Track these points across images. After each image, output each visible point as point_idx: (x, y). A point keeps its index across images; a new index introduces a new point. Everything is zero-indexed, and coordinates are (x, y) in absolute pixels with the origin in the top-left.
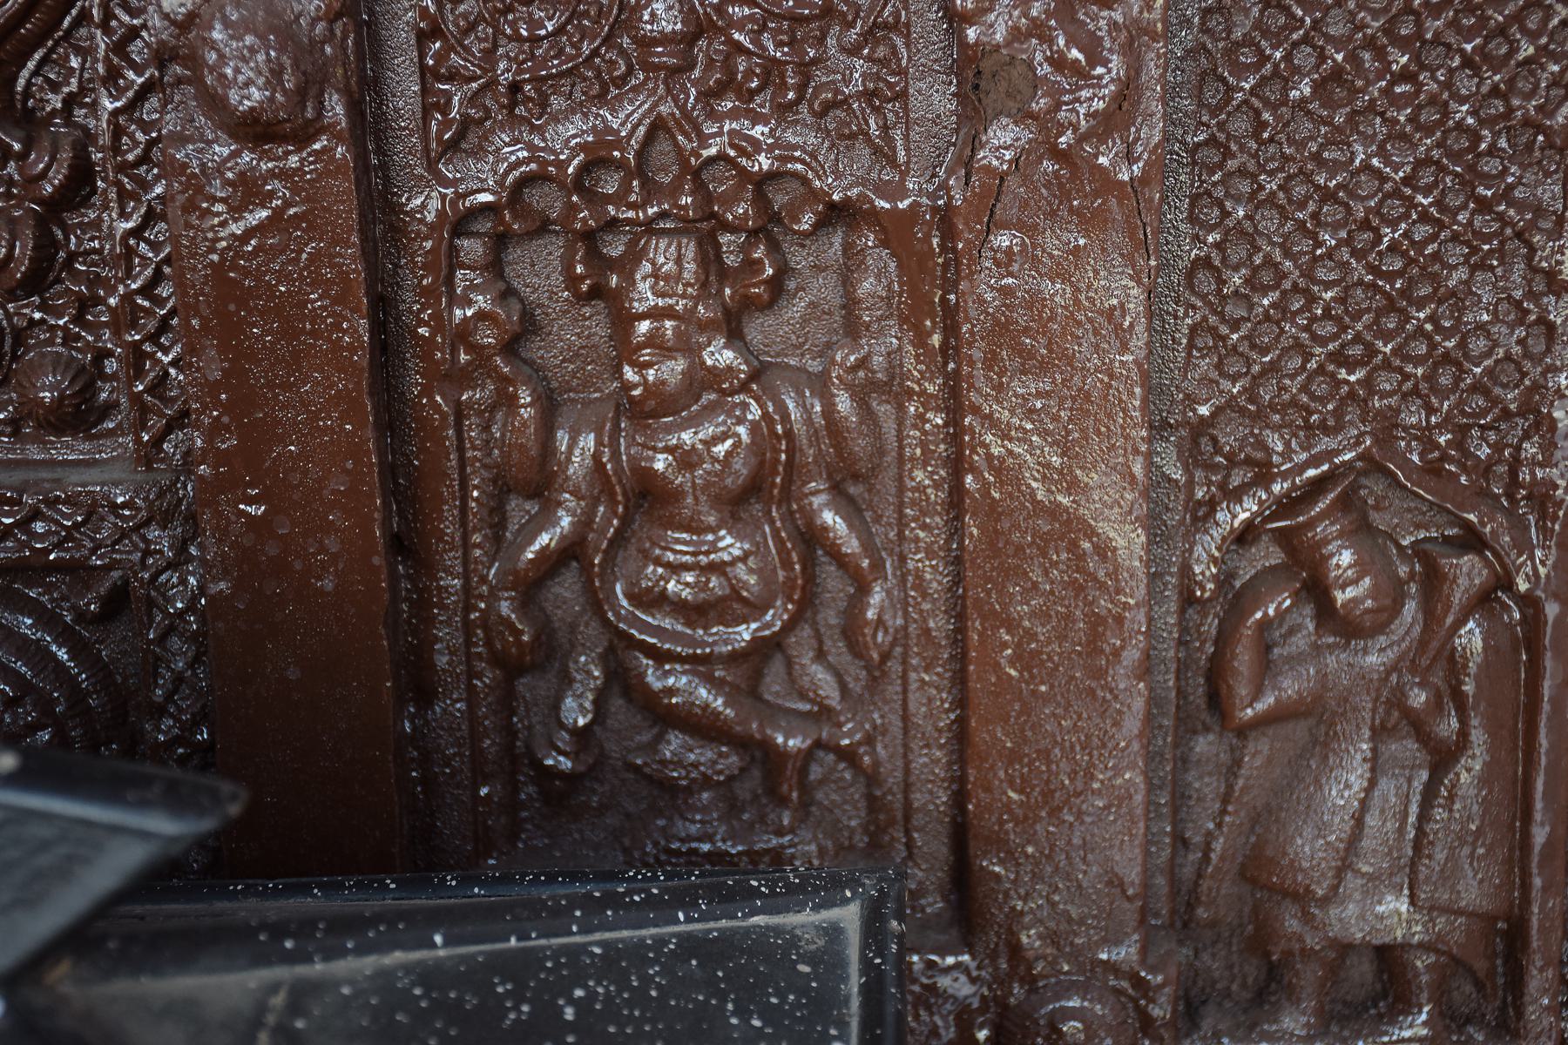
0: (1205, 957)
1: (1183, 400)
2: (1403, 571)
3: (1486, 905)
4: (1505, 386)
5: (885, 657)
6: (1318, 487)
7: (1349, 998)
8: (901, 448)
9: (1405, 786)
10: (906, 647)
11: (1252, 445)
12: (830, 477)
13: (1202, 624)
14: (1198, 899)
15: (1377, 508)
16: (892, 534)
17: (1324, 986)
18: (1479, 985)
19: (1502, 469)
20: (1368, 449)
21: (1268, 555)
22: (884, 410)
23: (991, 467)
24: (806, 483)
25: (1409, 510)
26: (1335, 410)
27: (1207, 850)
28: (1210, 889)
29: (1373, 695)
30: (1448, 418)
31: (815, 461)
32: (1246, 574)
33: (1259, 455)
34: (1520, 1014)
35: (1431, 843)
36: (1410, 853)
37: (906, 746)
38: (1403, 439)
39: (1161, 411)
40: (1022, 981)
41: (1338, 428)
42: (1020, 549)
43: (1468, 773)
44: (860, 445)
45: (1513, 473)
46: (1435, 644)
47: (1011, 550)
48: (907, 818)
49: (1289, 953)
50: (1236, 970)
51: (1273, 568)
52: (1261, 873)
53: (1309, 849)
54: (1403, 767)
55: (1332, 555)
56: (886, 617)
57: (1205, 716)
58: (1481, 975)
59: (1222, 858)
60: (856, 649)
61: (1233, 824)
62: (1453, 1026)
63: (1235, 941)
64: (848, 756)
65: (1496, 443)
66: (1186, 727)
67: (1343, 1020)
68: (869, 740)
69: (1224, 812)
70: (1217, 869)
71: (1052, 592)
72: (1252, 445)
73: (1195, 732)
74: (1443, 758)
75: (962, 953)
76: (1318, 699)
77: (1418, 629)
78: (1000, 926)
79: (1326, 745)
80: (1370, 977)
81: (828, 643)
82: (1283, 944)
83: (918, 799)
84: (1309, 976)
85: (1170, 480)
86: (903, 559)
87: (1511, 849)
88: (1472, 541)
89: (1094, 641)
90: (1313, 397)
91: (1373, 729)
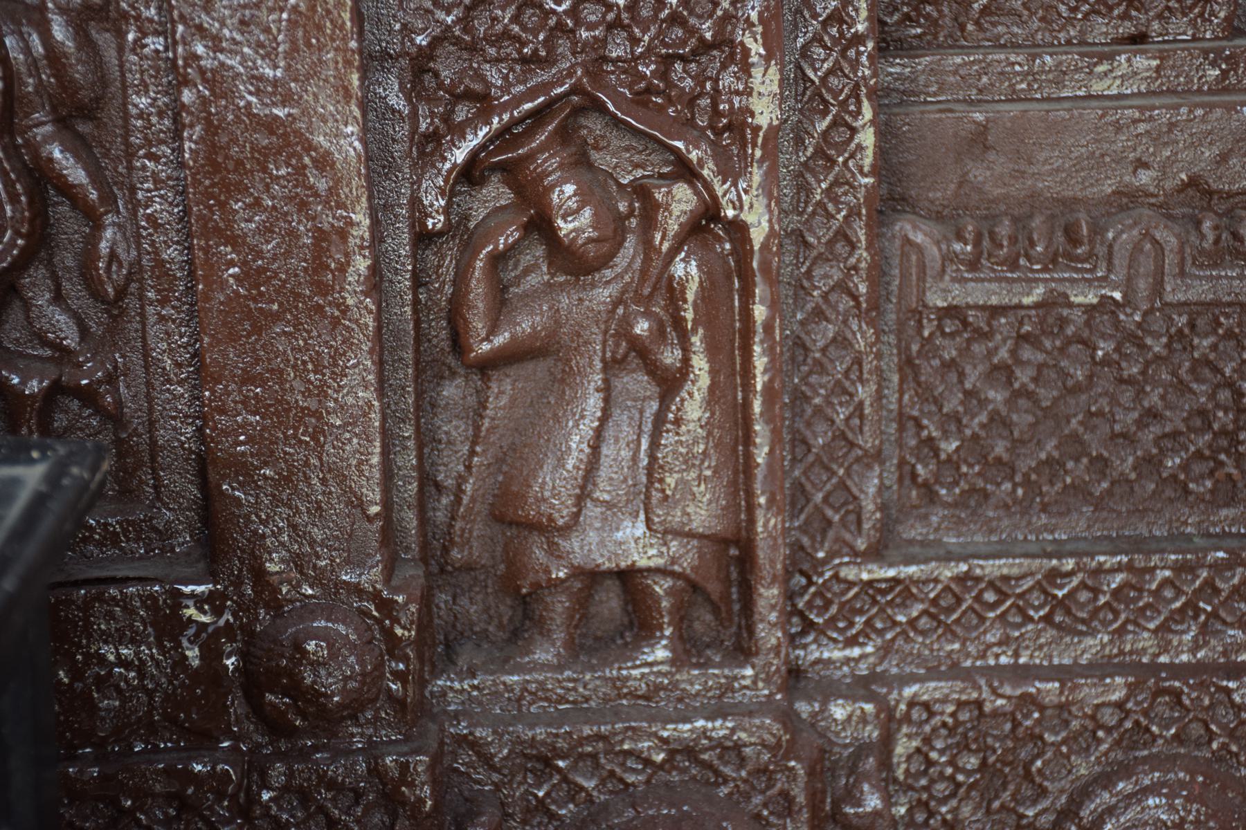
0: (464, 601)
1: (401, 31)
2: (622, 207)
3: (717, 527)
4: (700, 17)
5: (122, 293)
6: (538, 116)
7: (599, 633)
8: (123, 75)
9: (637, 416)
10: (141, 280)
11: (471, 77)
12: (54, 109)
13: (440, 266)
14: (451, 541)
15: (597, 148)
16: (120, 169)
17: (572, 617)
18: (716, 610)
19: (705, 102)
20: (580, 79)
21: (496, 193)
22: (105, 40)
23: (205, 81)
24: (27, 115)
25: (627, 149)
26: (546, 41)
27: (459, 492)
28: (463, 530)
29: (603, 327)
30: (649, 49)
31: (37, 92)
32: (479, 214)
33: (477, 87)
34: (751, 630)
35: (661, 467)
36: (644, 479)
37: (148, 384)
38: (613, 72)
39: (380, 41)
40: (267, 607)
41: (549, 61)
42: (239, 163)
43: (693, 406)
44: (79, 72)
45: (715, 105)
46: (654, 272)
47: (231, 166)
48: (153, 459)
49: (537, 586)
50: (492, 612)
51: (502, 208)
52: (514, 518)
53: (553, 486)
54: (635, 400)
55: (551, 188)
56: (119, 251)
57: (451, 360)
58: (715, 597)
59: (473, 499)
60: (96, 293)
61: (482, 464)
62: (694, 651)
63: (490, 582)
64: (88, 397)
65: (697, 75)
66: (428, 373)
67: (591, 651)
68: (111, 379)
69: (473, 453)
70: (469, 510)
71: (274, 207)
72: (471, 77)
73: (442, 378)
74: (670, 383)
75: (271, 703)
76: (553, 334)
77: (639, 261)
78: (243, 551)
79: (563, 381)
80: (618, 611)
81: (66, 285)
82: (531, 577)
83: (162, 436)
84: (560, 605)
85: (394, 111)
86: (133, 190)
87: (736, 472)
88: (686, 171)
89: (320, 257)
90: (524, 28)
91: (603, 360)
